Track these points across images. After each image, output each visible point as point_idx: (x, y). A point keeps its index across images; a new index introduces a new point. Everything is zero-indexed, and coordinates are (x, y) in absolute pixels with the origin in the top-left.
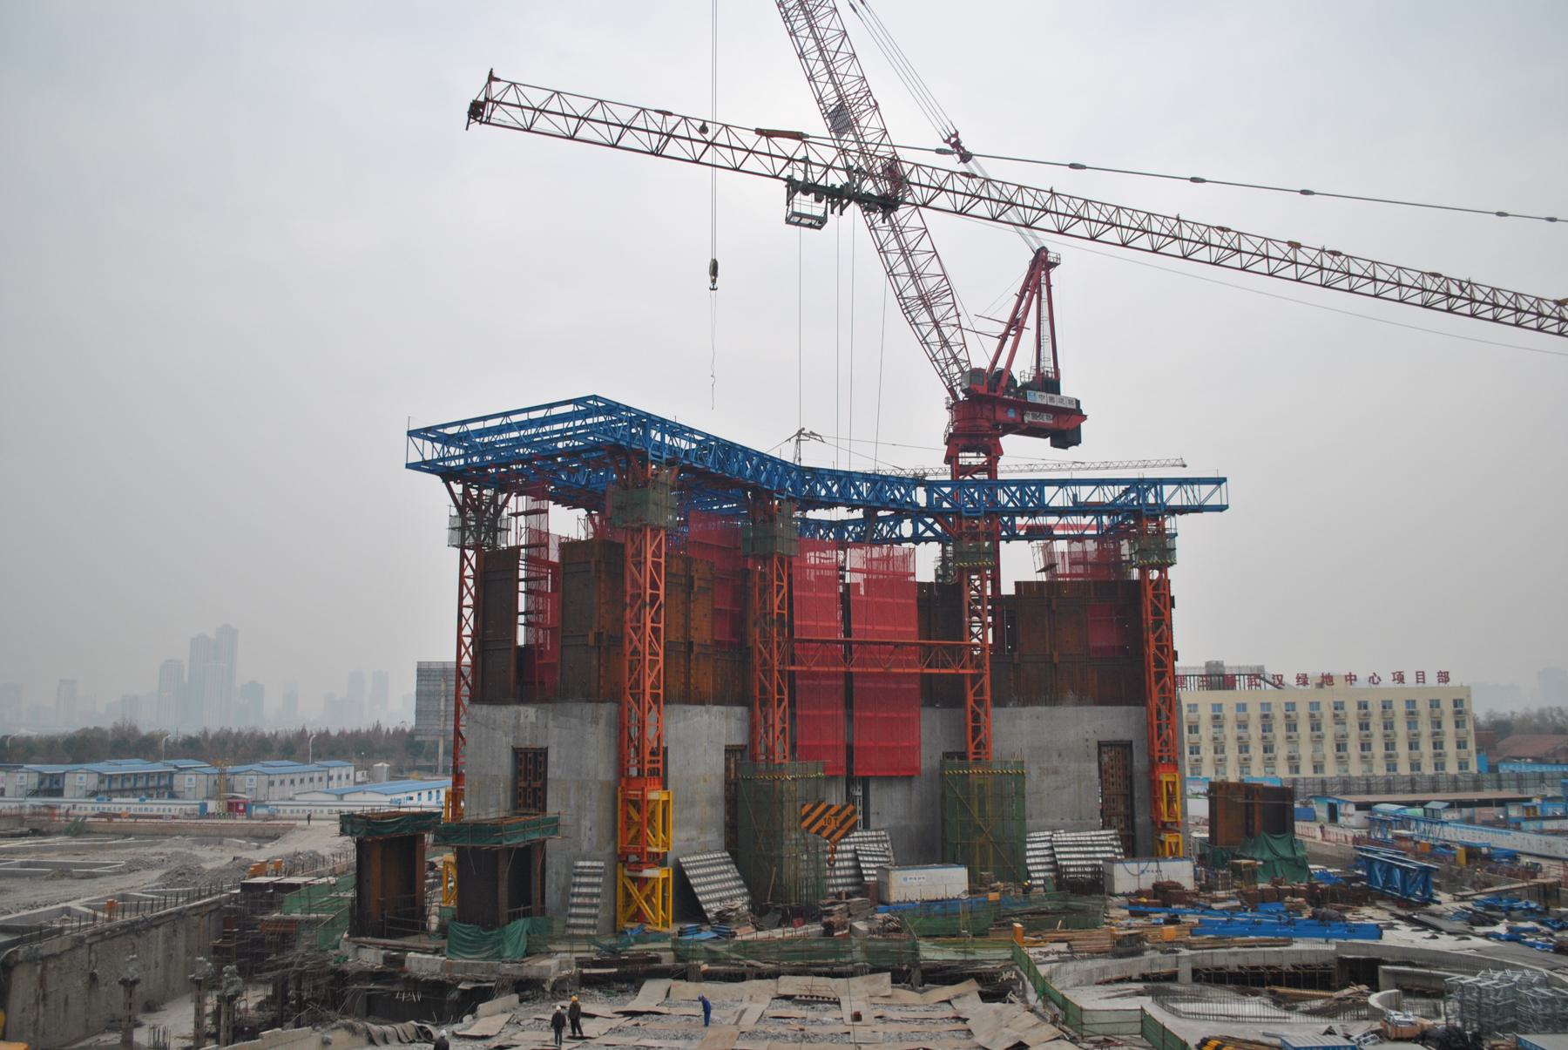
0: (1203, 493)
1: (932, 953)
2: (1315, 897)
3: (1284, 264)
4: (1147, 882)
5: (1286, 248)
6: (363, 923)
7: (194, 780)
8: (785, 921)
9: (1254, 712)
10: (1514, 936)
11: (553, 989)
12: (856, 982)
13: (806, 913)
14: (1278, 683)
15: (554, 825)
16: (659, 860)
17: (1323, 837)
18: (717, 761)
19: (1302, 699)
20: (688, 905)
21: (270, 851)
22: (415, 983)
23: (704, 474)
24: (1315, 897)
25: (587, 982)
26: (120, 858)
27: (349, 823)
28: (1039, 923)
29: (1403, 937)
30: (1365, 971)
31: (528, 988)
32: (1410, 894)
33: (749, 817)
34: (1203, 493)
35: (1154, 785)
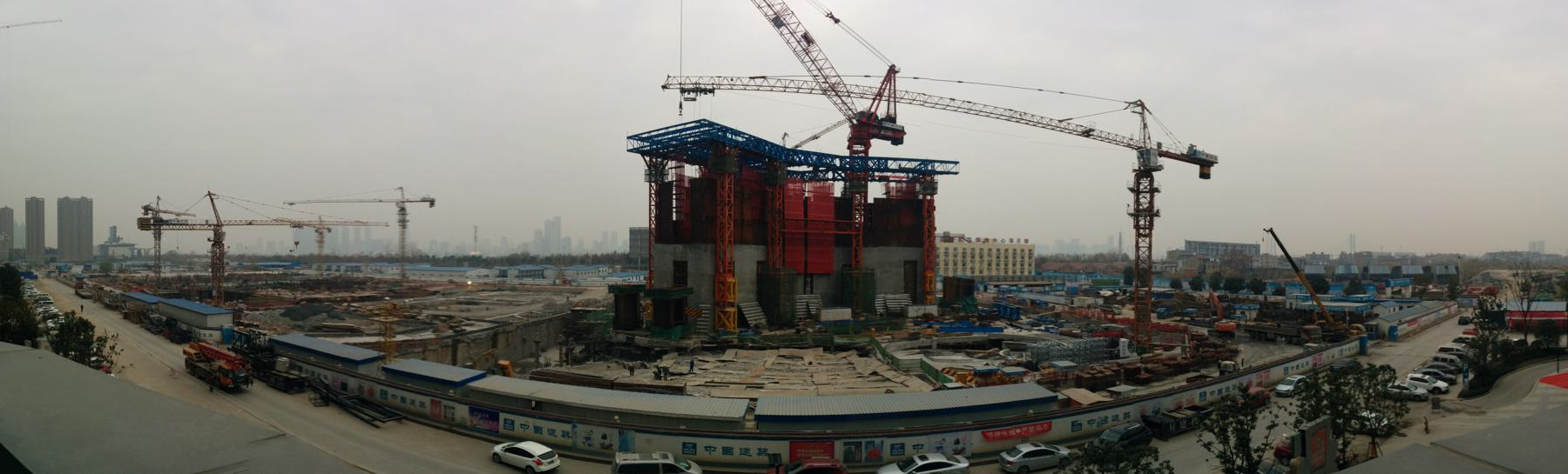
0: (950, 167)
1: (838, 340)
2: (980, 318)
4: (921, 313)
6: (618, 324)
7: (550, 272)
8: (781, 328)
9: (960, 251)
10: (1047, 330)
11: (868, 227)
12: (810, 351)
13: (791, 326)
14: (969, 241)
15: (691, 291)
16: (732, 305)
17: (984, 297)
18: (754, 267)
19: (977, 246)
20: (742, 321)
21: (578, 298)
22: (638, 347)
23: (749, 151)
24: (980, 318)
25: (705, 349)
26: (529, 299)
27: (612, 288)
28: (880, 329)
29: (1010, 331)
30: (998, 343)
31: (682, 351)
32: (1012, 317)
33: (768, 289)
34: (950, 167)
35: (924, 277)
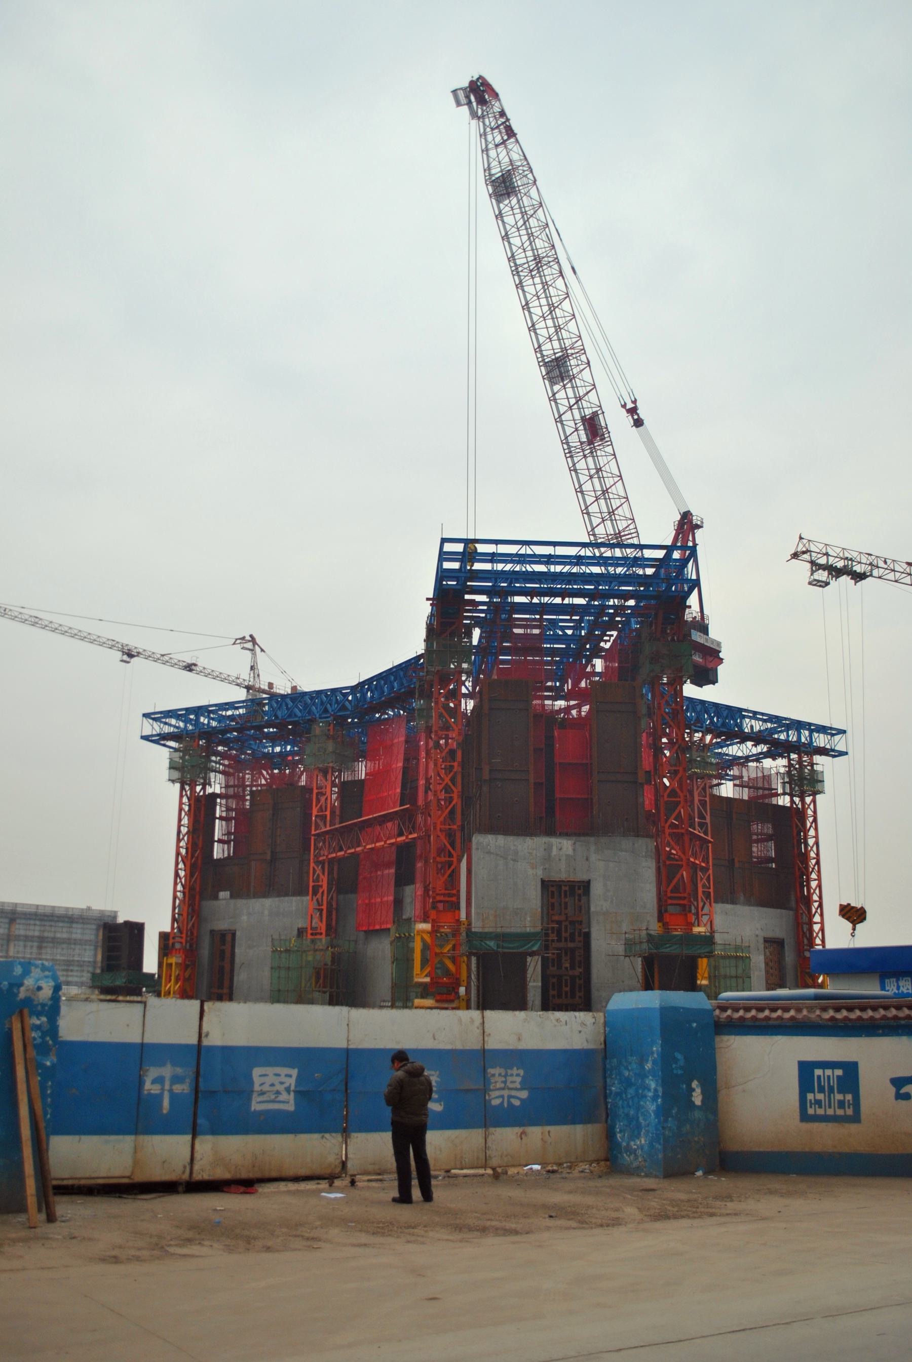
3: (904, 575)
5: (905, 566)
